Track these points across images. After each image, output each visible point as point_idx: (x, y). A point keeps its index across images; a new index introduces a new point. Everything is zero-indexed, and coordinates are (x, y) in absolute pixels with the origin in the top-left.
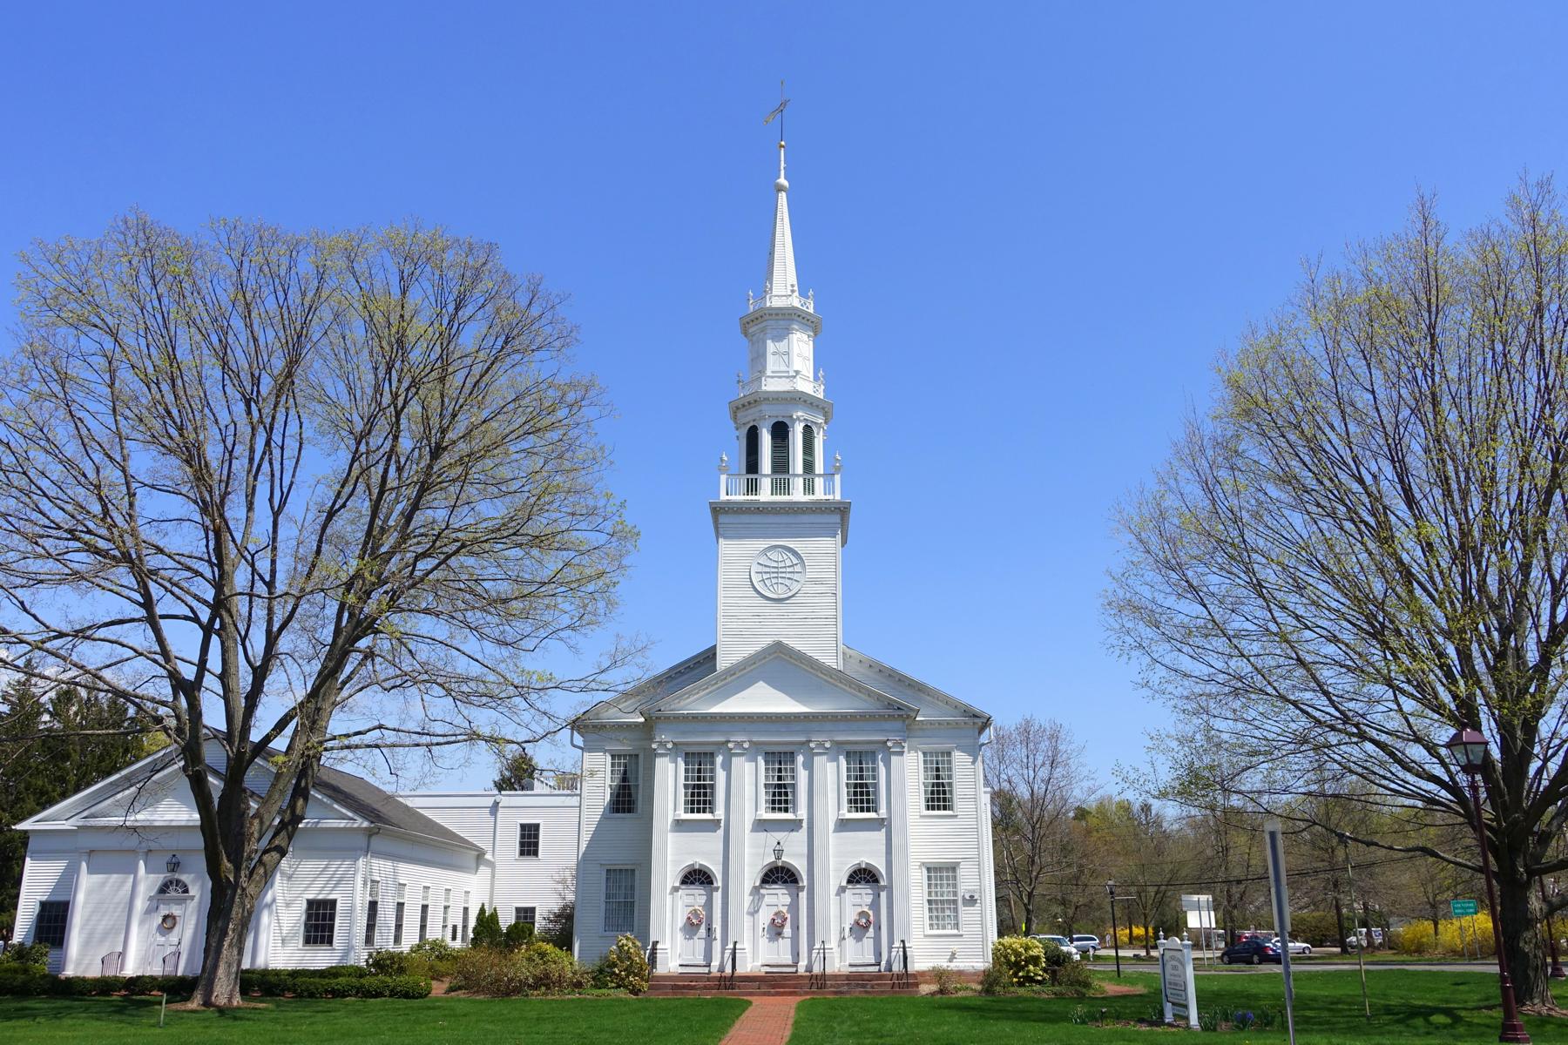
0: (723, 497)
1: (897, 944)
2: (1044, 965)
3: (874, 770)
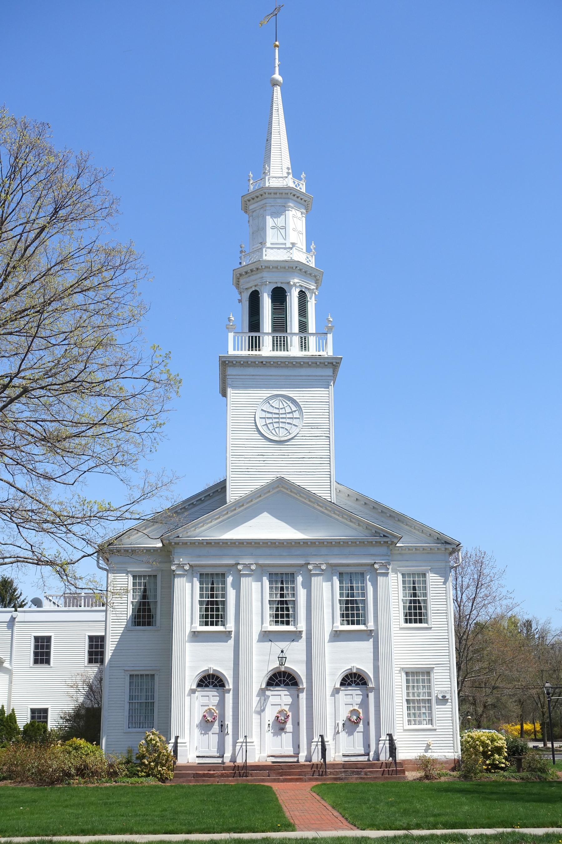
0: (231, 352)
1: (316, 738)
2: (506, 754)
3: (363, 588)
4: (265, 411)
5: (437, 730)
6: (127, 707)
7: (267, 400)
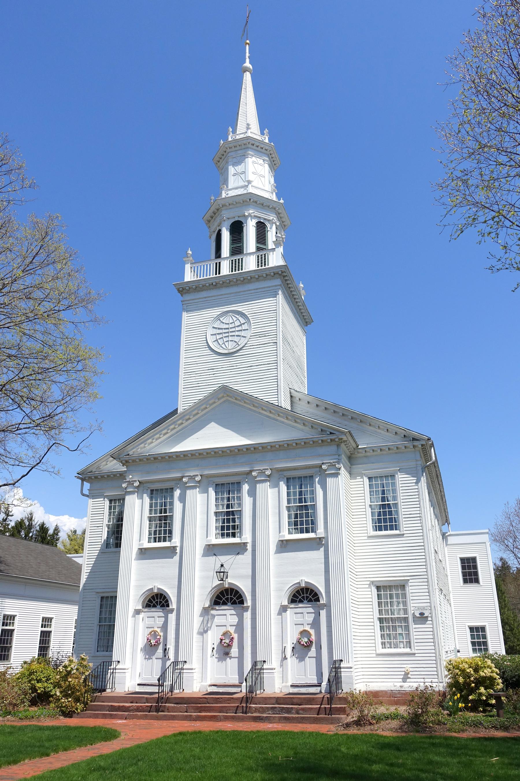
4: (216, 328)
5: (416, 655)
6: (96, 629)
7: (218, 318)
